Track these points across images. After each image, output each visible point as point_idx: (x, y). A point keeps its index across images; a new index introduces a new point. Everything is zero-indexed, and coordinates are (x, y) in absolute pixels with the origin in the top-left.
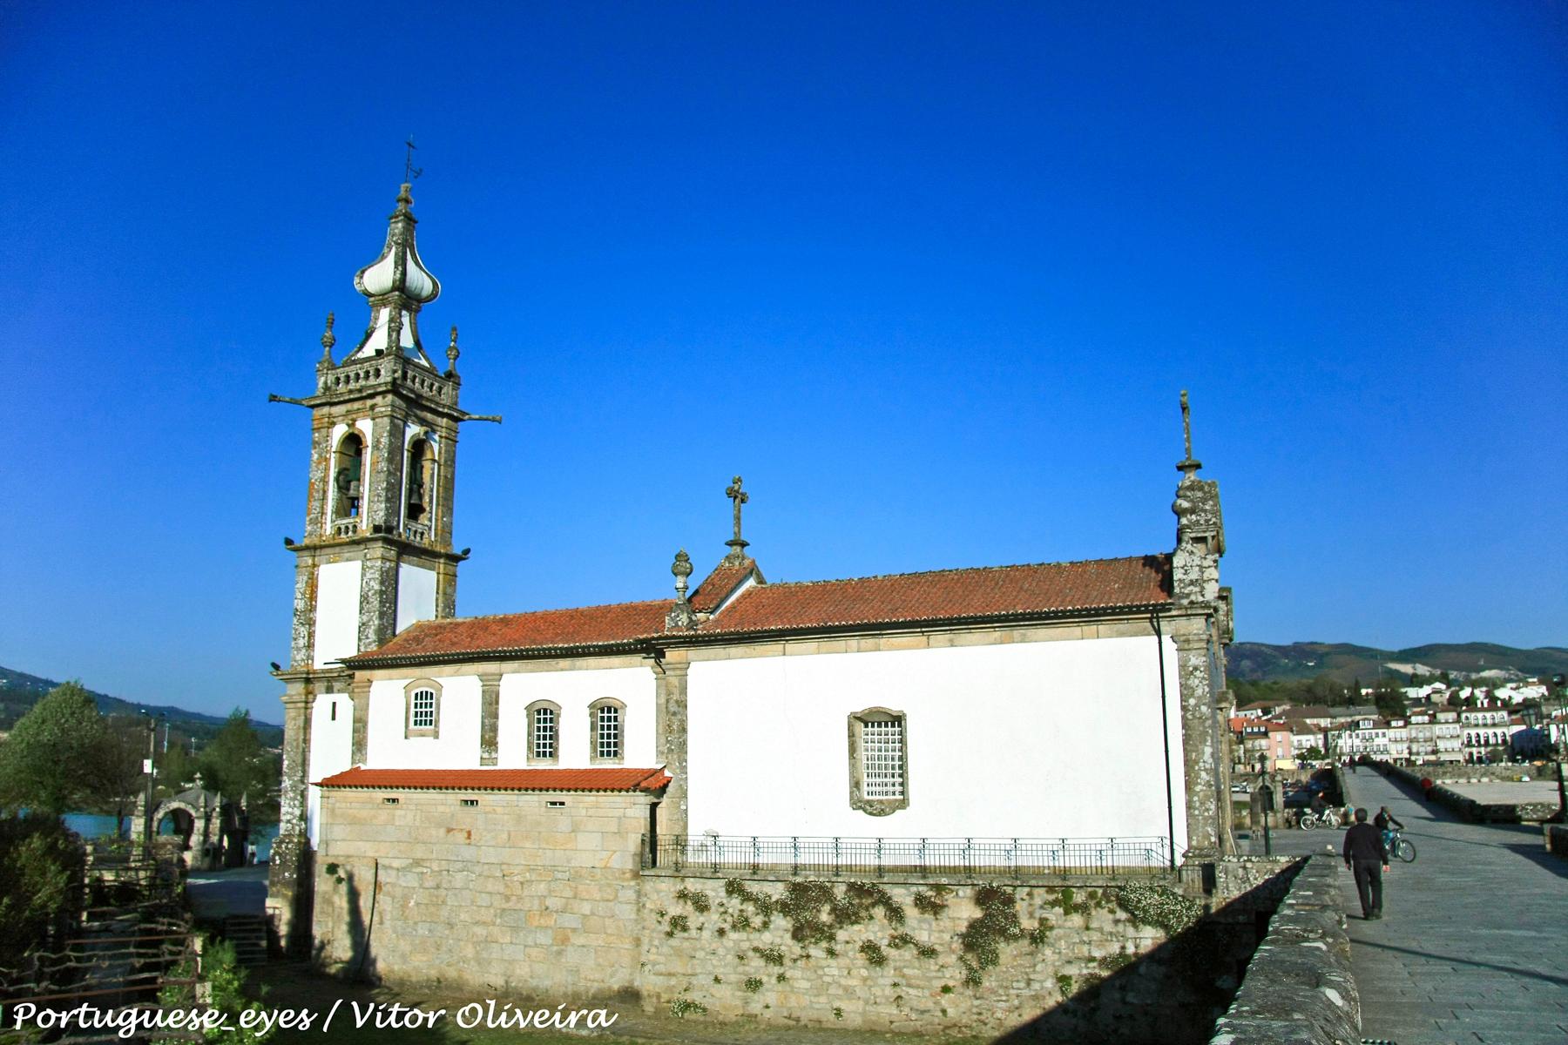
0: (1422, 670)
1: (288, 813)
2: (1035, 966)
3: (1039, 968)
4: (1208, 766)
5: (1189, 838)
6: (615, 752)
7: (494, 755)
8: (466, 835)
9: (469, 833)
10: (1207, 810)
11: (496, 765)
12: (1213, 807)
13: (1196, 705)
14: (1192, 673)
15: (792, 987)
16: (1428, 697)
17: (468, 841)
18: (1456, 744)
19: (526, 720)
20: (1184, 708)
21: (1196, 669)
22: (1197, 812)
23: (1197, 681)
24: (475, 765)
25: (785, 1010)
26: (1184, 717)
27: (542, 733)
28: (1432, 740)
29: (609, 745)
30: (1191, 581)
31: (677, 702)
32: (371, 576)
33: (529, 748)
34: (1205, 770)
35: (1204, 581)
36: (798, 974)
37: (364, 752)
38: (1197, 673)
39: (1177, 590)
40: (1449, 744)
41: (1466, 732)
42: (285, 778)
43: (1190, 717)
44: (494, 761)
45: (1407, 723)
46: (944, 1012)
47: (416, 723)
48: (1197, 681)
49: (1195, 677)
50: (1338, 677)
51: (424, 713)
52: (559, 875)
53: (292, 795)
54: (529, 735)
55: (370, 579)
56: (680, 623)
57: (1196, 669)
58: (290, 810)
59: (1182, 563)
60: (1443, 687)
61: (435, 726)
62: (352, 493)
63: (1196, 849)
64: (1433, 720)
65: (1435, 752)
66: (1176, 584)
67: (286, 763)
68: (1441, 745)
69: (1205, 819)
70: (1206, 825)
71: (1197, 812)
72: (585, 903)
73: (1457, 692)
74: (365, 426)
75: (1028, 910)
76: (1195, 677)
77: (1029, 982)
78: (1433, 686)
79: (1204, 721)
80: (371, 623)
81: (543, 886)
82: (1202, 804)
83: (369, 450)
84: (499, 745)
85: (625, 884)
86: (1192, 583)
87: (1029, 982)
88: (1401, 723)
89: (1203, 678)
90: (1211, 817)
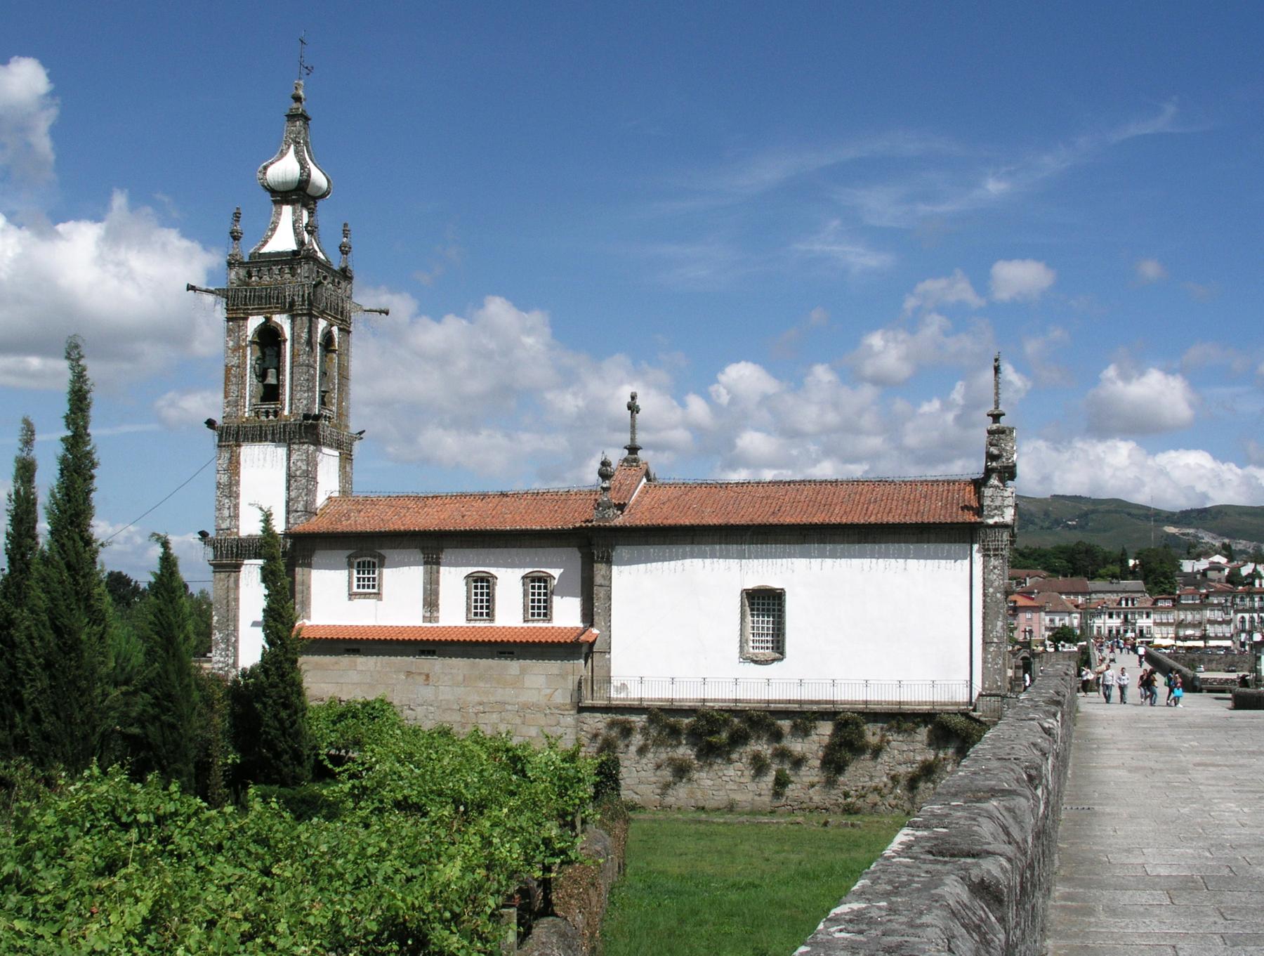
0: (1207, 538)
1: (219, 661)
2: (875, 767)
3: (878, 768)
4: (999, 635)
5: (983, 683)
6: (488, 614)
7: (435, 614)
8: (424, 677)
9: (428, 676)
10: (997, 664)
11: (550, 620)
12: (1000, 662)
13: (993, 592)
14: (992, 570)
15: (699, 785)
16: (1204, 573)
17: (426, 683)
18: (1228, 630)
19: (465, 588)
20: (985, 595)
21: (995, 568)
22: (989, 665)
23: (995, 576)
24: (419, 622)
25: (693, 801)
26: (984, 601)
27: (479, 597)
28: (1200, 623)
29: (539, 608)
30: (996, 506)
31: (603, 576)
32: (298, 458)
33: (468, 610)
34: (997, 637)
35: (1005, 507)
36: (703, 775)
37: (308, 610)
38: (996, 571)
39: (985, 513)
40: (1220, 630)
41: (1240, 615)
42: (216, 631)
43: (989, 601)
44: (437, 620)
45: (1177, 604)
46: (811, 799)
47: (358, 587)
48: (995, 576)
49: (994, 574)
50: (1105, 543)
51: (482, 586)
52: (509, 707)
53: (223, 646)
54: (468, 598)
55: (298, 461)
56: (606, 516)
57: (995, 568)
58: (222, 659)
59: (990, 494)
60: (1223, 560)
61: (379, 590)
62: (271, 380)
63: (988, 690)
64: (1204, 605)
65: (1204, 637)
66: (985, 508)
67: (215, 618)
68: (1211, 630)
69: (995, 670)
70: (994, 674)
71: (989, 665)
72: (532, 728)
73: (1239, 568)
74: (282, 321)
75: (872, 733)
76: (994, 574)
77: (871, 778)
78: (1211, 559)
79: (998, 604)
80: (300, 499)
81: (495, 716)
82: (993, 660)
83: (288, 344)
84: (440, 607)
85: (566, 713)
86: (996, 508)
87: (871, 778)
88: (1169, 604)
89: (1000, 575)
90: (998, 669)
